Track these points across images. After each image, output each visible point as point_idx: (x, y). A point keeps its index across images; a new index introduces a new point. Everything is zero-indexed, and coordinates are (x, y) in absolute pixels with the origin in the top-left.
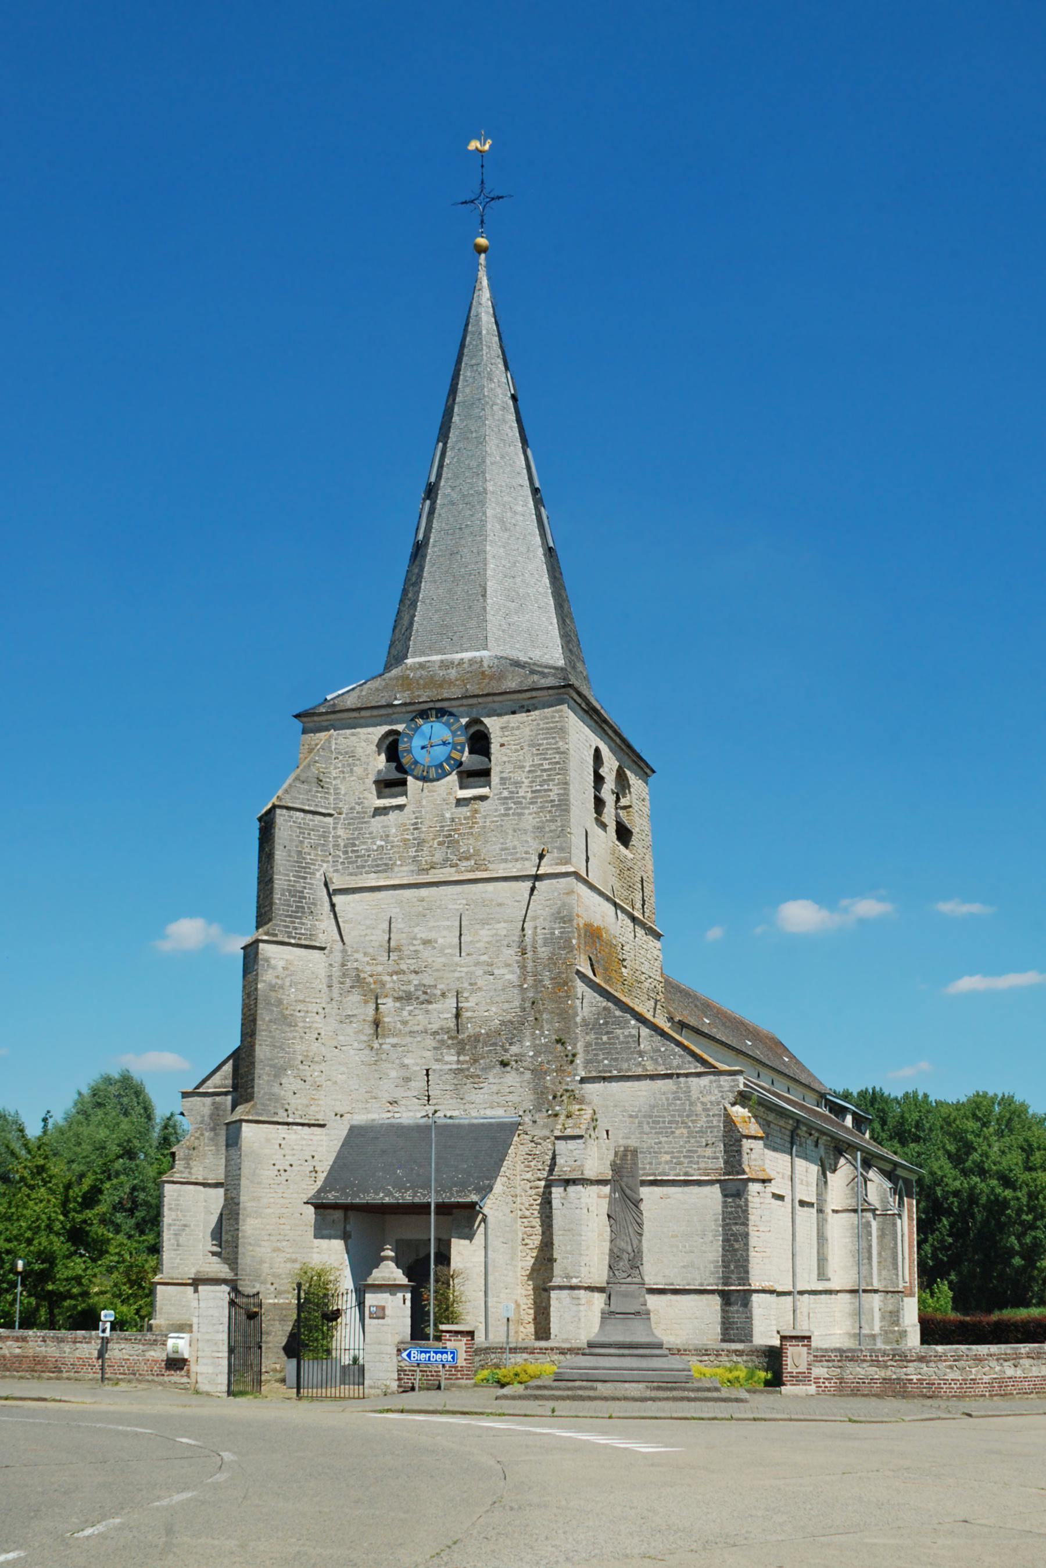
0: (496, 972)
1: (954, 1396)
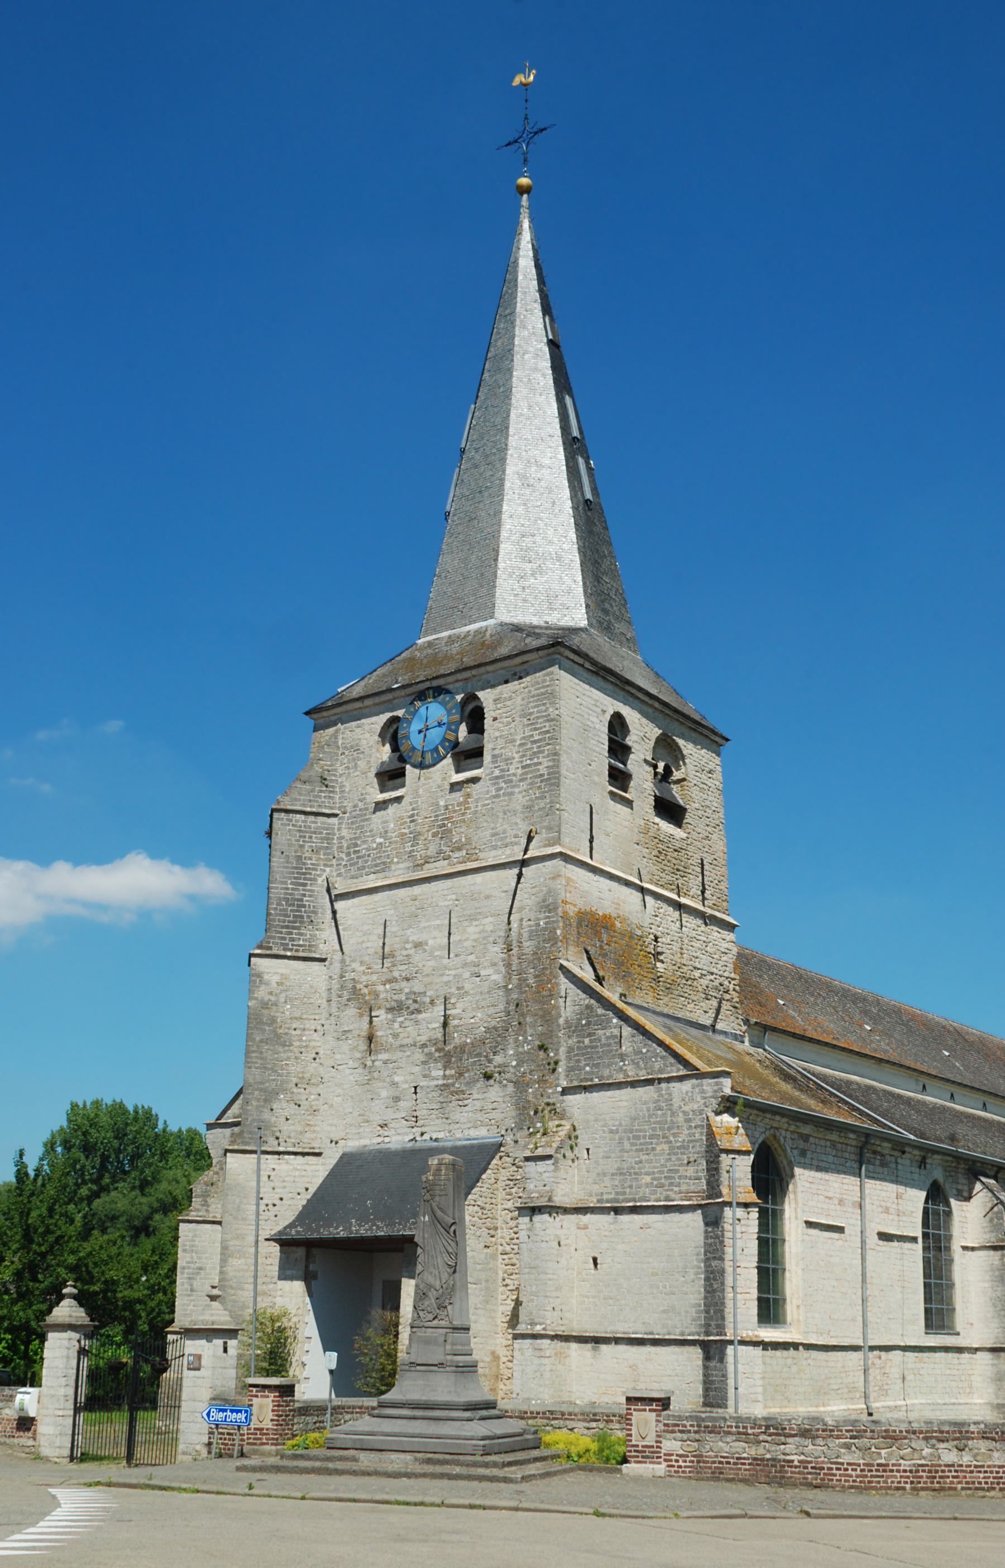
0: (483, 973)
1: (852, 1487)
